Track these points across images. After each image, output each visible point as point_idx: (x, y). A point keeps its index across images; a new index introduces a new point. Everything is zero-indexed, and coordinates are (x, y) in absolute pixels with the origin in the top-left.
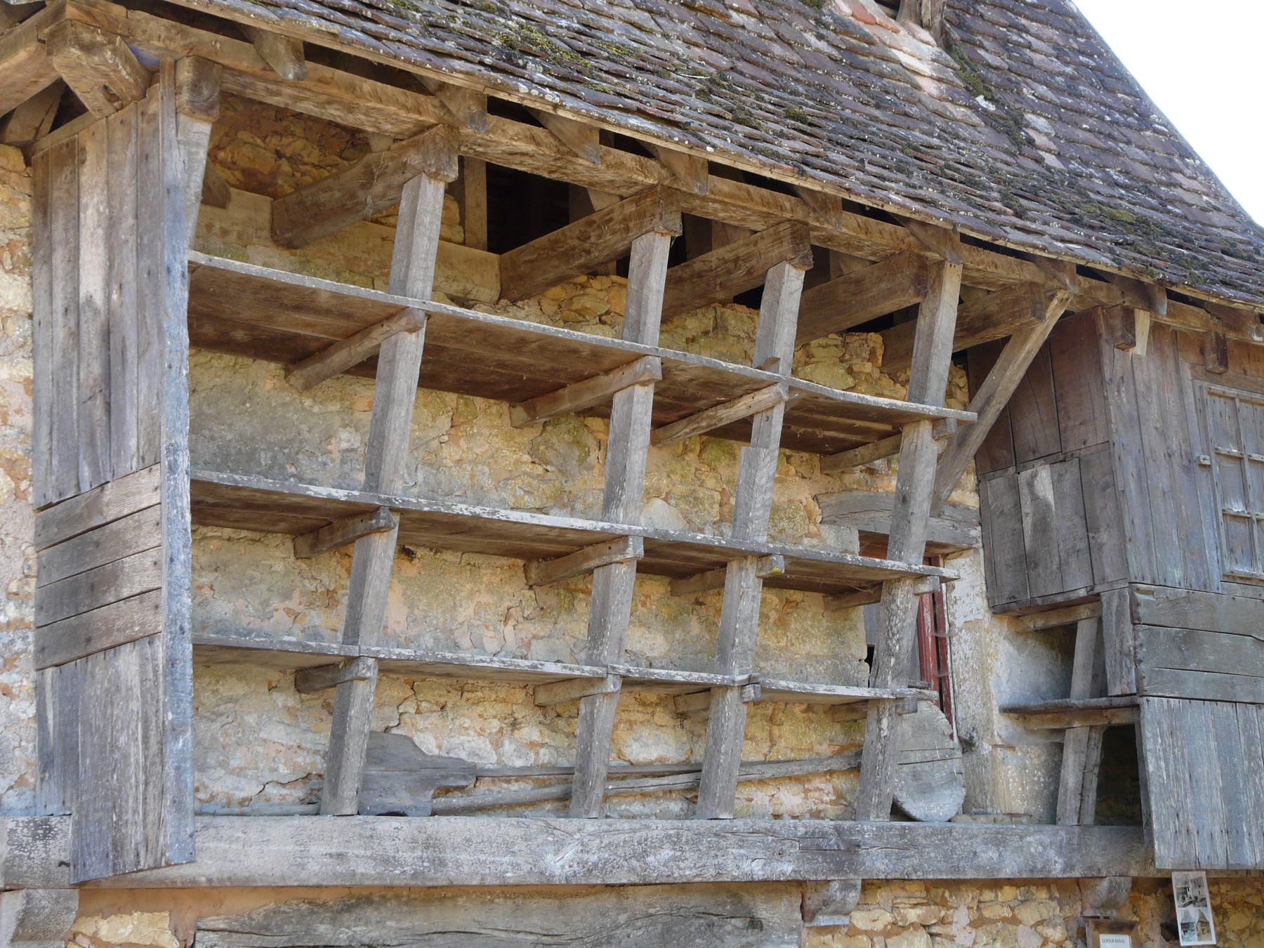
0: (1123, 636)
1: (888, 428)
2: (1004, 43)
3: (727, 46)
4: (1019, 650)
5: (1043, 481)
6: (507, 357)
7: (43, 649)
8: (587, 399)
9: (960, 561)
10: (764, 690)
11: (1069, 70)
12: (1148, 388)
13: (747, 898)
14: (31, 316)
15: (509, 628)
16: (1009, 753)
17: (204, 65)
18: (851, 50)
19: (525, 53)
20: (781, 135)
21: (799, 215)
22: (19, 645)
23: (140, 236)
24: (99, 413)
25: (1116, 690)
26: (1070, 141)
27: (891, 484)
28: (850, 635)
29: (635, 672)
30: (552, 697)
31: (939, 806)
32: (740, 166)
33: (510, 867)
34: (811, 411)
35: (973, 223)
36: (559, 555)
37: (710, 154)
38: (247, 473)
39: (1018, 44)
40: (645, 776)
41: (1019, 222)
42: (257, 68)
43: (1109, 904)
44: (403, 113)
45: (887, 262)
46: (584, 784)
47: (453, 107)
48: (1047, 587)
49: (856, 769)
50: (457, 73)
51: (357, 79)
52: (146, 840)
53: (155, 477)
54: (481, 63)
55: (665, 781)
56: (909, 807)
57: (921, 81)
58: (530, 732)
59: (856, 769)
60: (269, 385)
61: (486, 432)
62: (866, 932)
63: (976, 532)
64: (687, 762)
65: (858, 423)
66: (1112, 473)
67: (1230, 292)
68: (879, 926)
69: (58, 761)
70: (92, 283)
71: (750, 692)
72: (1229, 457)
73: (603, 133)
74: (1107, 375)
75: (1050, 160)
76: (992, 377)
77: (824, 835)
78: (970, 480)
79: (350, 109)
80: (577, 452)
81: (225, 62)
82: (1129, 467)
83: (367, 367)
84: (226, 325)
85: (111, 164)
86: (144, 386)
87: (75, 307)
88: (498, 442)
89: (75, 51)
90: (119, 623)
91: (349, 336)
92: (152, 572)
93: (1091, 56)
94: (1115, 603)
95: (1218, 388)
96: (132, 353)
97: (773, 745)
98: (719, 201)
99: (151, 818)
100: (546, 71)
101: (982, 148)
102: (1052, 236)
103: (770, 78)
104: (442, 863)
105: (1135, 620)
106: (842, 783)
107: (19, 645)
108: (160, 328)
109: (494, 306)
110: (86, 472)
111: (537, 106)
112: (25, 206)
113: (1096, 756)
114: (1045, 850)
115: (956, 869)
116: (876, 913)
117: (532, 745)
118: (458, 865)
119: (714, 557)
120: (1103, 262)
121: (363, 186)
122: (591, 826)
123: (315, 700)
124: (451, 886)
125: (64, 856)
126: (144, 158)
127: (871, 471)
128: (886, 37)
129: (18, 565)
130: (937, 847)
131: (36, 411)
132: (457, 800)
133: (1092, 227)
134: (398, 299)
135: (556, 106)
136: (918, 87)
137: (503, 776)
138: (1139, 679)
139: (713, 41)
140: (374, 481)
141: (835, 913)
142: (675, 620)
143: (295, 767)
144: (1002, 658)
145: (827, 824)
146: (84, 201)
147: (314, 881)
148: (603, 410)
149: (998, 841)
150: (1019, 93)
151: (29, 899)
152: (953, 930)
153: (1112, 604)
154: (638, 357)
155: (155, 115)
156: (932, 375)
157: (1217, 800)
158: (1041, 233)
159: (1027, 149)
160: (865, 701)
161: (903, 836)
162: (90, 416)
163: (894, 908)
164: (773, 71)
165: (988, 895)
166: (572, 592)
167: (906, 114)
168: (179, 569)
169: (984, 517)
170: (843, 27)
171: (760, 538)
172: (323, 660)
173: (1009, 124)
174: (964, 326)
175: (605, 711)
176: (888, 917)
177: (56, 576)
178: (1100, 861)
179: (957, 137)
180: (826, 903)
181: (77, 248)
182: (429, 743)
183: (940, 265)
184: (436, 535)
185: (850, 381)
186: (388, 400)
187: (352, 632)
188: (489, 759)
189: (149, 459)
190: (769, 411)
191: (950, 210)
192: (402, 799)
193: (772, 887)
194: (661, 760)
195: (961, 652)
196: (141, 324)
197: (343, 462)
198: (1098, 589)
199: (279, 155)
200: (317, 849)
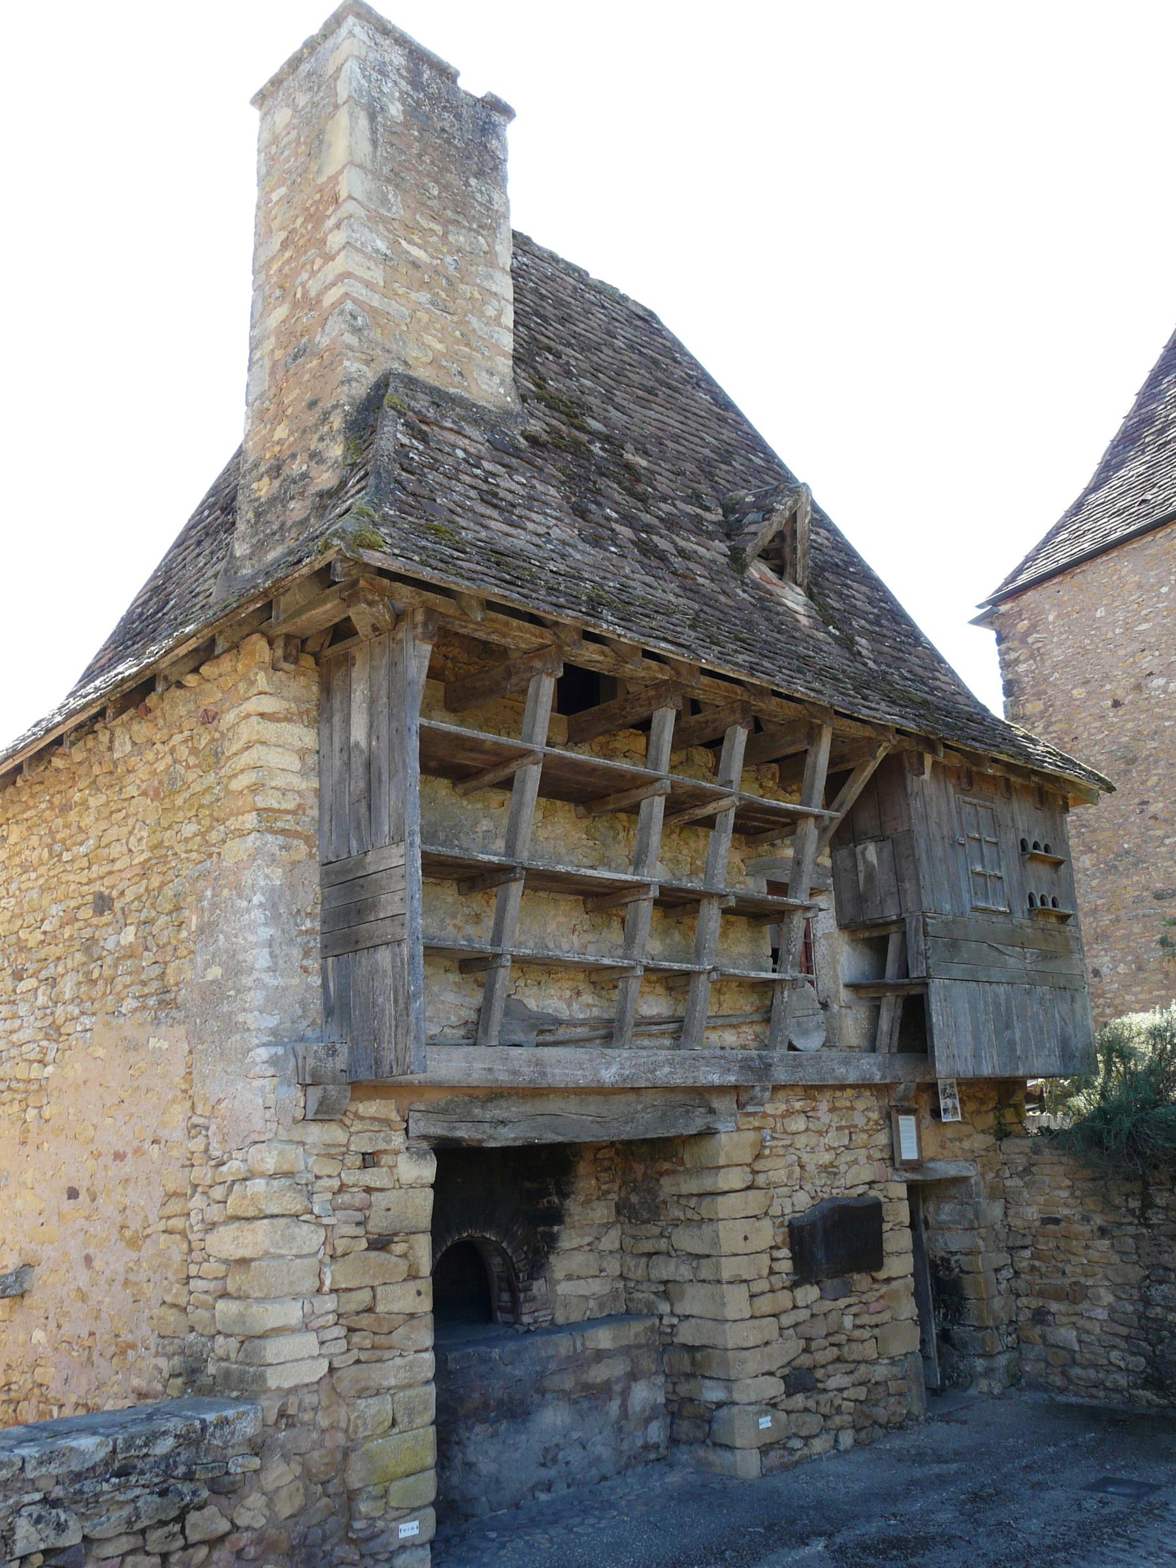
0: (918, 943)
1: (788, 820)
2: (840, 594)
3: (696, 597)
4: (854, 950)
5: (871, 852)
6: (581, 778)
7: (326, 947)
8: (625, 803)
9: (820, 898)
10: (722, 975)
11: (876, 611)
12: (931, 799)
13: (707, 1096)
14: (318, 752)
15: (575, 937)
16: (849, 1011)
17: (430, 612)
18: (761, 599)
19: (600, 604)
20: (736, 651)
21: (745, 698)
22: (312, 944)
23: (390, 708)
24: (363, 809)
25: (914, 974)
26: (880, 653)
27: (790, 853)
28: (762, 941)
29: (652, 964)
30: (599, 977)
31: (812, 1042)
32: (717, 670)
33: (581, 1077)
34: (748, 811)
35: (842, 704)
36: (607, 894)
37: (703, 664)
38: (432, 845)
39: (847, 596)
40: (650, 1024)
41: (866, 703)
42: (458, 613)
43: (904, 1098)
44: (534, 639)
45: (791, 725)
46: (621, 1029)
47: (562, 636)
48: (872, 913)
49: (768, 1021)
50: (568, 617)
51: (510, 619)
52: (397, 1059)
53: (402, 849)
54: (580, 611)
55: (663, 1027)
56: (795, 1043)
57: (798, 616)
58: (587, 998)
59: (768, 1021)
60: (444, 793)
61: (562, 821)
62: (772, 1116)
63: (830, 881)
64: (673, 1016)
65: (773, 818)
66: (913, 848)
67: (977, 745)
68: (779, 1112)
69: (337, 1012)
70: (359, 734)
71: (714, 975)
72: (974, 839)
73: (644, 651)
74: (909, 791)
75: (871, 664)
76: (844, 790)
77: (752, 1059)
78: (827, 850)
79: (504, 636)
80: (612, 833)
81: (441, 610)
82: (922, 845)
83: (507, 784)
84: (447, 764)
85: (372, 667)
86: (393, 796)
87: (347, 748)
88: (569, 827)
89: (364, 605)
90: (378, 933)
91: (495, 766)
92: (399, 904)
93: (886, 603)
94: (914, 924)
95: (967, 799)
96: (385, 777)
97: (720, 1005)
98: (702, 688)
99: (400, 1046)
100: (612, 615)
101: (834, 657)
102: (889, 715)
103: (721, 616)
104: (545, 1074)
105: (926, 934)
106: (758, 1028)
107: (312, 944)
108: (404, 762)
109: (565, 745)
110: (354, 844)
111: (609, 635)
112: (315, 688)
113: (899, 1012)
114: (870, 1067)
115: (823, 1079)
116: (778, 1105)
117: (588, 1005)
118: (554, 1076)
119: (694, 896)
120: (911, 726)
121: (504, 679)
122: (626, 1054)
123: (470, 978)
124: (550, 1088)
125: (343, 1067)
126: (393, 664)
127: (773, 845)
128: (779, 591)
129: (311, 897)
130: (812, 1066)
131: (321, 808)
132: (549, 1038)
133: (901, 705)
134: (529, 746)
135: (619, 636)
136: (798, 621)
137: (572, 1023)
138: (928, 968)
139: (691, 595)
140: (511, 849)
141: (756, 1105)
142: (666, 933)
143: (460, 1017)
144: (845, 954)
145: (754, 1053)
146: (354, 687)
147: (476, 1084)
148: (634, 810)
149: (846, 1062)
150: (851, 624)
151: (325, 1090)
152: (819, 1114)
153: (911, 925)
154: (657, 779)
155: (401, 640)
156: (815, 791)
157: (969, 1038)
158: (877, 710)
159: (858, 657)
160: (774, 981)
161: (795, 1060)
162: (357, 812)
163: (787, 1101)
164: (722, 612)
165: (838, 1094)
166: (610, 916)
167: (794, 637)
168: (416, 903)
169: (834, 872)
170: (756, 586)
171: (720, 886)
172: (481, 955)
173: (847, 643)
174: (832, 763)
175: (634, 986)
176: (784, 1107)
177: (334, 904)
178: (900, 1073)
179: (821, 650)
180: (752, 1099)
181: (349, 714)
182: (532, 1004)
183: (820, 726)
184: (546, 883)
185: (761, 792)
186: (520, 804)
187: (497, 939)
188: (565, 1014)
189: (397, 838)
190: (726, 811)
191: (829, 697)
192: (519, 1037)
193: (722, 1090)
194: (658, 1015)
195: (820, 951)
196: (391, 760)
197: (484, 838)
198: (904, 916)
199: (446, 657)
200: (478, 1065)
